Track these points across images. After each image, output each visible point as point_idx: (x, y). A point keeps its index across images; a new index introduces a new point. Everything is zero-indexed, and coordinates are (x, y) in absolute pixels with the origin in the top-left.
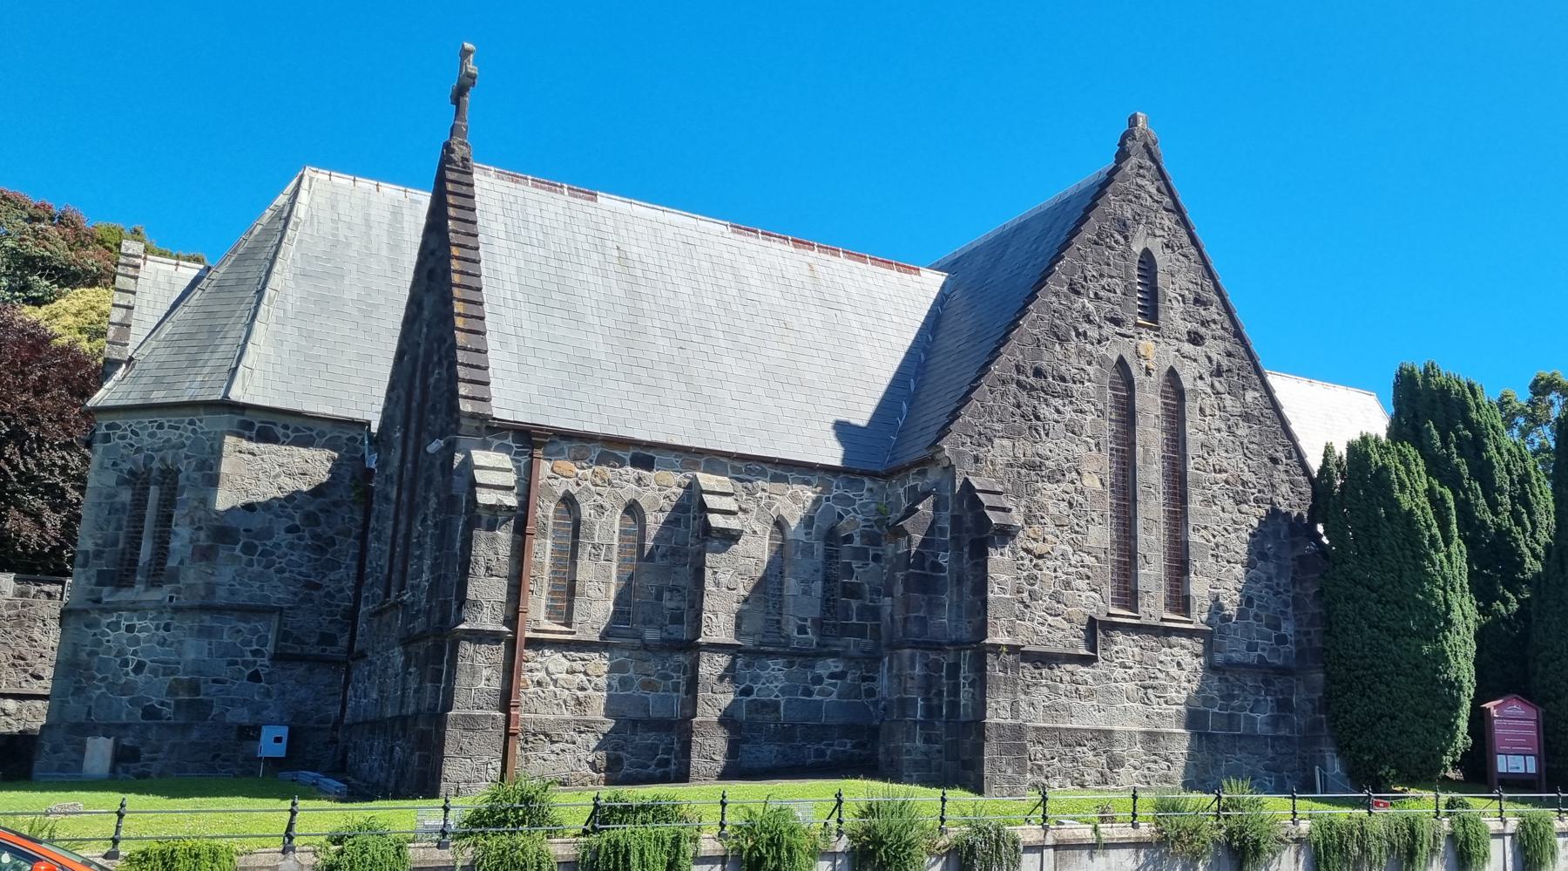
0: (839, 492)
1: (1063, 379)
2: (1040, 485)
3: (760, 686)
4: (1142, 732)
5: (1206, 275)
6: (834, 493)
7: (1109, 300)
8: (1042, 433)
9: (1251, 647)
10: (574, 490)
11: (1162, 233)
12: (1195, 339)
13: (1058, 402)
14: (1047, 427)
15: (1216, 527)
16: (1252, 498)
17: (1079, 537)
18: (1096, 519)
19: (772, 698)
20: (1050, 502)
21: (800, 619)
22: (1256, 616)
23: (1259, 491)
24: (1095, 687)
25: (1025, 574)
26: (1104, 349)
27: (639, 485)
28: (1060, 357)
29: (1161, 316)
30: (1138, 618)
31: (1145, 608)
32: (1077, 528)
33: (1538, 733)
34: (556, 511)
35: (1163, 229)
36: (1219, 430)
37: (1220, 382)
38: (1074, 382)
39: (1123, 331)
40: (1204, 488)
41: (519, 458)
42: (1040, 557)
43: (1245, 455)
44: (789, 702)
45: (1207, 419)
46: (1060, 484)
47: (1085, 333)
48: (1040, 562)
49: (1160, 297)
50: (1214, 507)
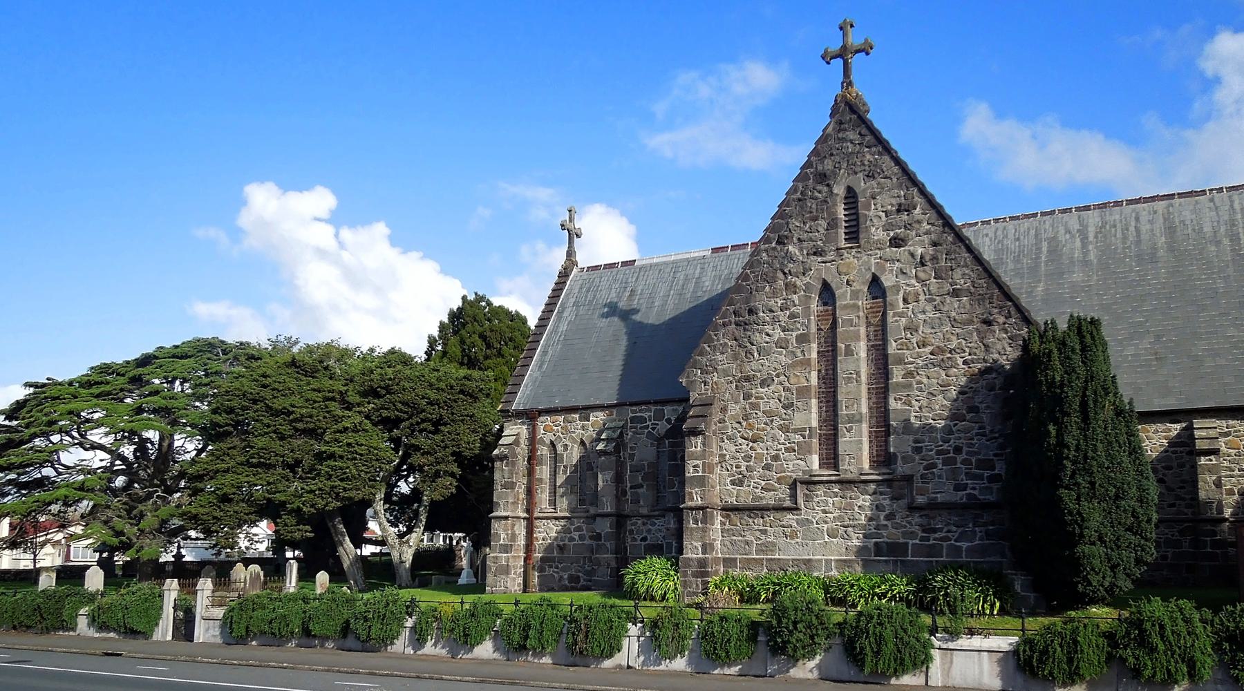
1: (772, 311)
2: (753, 392)
4: (837, 561)
5: (909, 184)
7: (811, 240)
9: (957, 488)
10: (553, 438)
11: (863, 168)
12: (897, 242)
15: (919, 393)
16: (960, 361)
18: (801, 407)
20: (761, 401)
23: (970, 354)
25: (743, 455)
26: (808, 279)
28: (770, 295)
29: (861, 236)
30: (839, 475)
31: (845, 467)
32: (784, 416)
35: (864, 164)
36: (924, 312)
37: (924, 271)
38: (781, 310)
40: (905, 364)
42: (754, 441)
45: (910, 306)
47: (790, 271)
48: (755, 445)
49: (862, 220)
50: (918, 377)
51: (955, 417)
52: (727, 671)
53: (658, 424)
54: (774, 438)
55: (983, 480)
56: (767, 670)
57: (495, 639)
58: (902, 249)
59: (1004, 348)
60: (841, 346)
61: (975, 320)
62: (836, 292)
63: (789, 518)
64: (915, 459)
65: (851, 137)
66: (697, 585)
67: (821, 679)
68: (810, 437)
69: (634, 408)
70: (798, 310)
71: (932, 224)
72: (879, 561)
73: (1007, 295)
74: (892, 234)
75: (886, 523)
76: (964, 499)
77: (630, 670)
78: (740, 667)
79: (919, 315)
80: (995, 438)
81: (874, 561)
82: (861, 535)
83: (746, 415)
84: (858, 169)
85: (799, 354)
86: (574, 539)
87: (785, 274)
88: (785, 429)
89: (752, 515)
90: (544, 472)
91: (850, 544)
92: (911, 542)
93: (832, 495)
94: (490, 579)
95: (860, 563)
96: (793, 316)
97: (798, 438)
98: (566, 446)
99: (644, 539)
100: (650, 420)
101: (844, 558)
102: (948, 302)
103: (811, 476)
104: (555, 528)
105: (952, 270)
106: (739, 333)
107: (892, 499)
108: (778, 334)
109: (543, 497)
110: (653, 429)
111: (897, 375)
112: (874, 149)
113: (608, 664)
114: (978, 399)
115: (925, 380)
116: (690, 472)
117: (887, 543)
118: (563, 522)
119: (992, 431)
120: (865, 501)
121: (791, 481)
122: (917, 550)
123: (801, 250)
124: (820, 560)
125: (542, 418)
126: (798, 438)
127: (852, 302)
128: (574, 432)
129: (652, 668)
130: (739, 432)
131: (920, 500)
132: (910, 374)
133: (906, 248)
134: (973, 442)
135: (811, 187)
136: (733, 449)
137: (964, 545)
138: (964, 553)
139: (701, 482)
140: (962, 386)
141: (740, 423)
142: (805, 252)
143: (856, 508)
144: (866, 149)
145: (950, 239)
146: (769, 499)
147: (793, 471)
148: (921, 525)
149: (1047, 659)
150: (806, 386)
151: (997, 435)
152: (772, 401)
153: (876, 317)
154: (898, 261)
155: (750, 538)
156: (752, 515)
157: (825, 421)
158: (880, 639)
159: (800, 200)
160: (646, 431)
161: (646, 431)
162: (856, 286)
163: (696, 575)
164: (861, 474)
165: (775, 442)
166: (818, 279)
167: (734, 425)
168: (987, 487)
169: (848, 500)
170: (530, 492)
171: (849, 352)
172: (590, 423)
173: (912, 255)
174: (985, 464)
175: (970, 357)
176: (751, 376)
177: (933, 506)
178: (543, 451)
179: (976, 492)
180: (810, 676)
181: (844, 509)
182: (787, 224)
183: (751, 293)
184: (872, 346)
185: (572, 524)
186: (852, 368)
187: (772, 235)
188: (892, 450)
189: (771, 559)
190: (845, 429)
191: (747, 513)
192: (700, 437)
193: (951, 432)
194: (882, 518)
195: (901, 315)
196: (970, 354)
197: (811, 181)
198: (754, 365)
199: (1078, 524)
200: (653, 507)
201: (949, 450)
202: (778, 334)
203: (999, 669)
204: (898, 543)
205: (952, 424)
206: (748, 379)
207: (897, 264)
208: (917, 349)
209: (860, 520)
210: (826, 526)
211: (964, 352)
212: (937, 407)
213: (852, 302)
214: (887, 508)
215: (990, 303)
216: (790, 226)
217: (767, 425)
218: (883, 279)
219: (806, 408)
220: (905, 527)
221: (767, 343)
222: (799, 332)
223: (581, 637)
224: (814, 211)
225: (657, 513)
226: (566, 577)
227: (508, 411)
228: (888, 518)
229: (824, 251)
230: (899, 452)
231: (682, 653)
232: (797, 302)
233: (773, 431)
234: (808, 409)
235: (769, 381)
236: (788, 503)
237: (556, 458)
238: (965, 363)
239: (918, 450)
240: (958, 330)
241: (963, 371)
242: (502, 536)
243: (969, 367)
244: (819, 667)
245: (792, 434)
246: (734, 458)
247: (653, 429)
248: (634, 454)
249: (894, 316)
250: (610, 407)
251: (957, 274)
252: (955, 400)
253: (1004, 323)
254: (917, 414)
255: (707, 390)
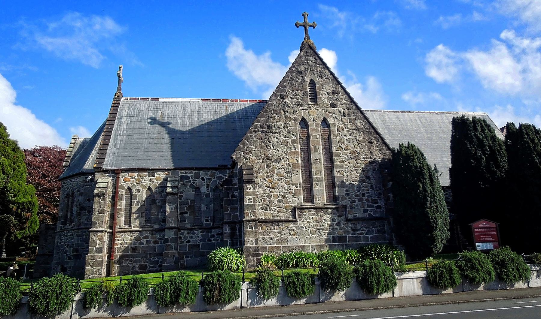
0: (218, 175)
3: (193, 240)
4: (317, 246)
5: (337, 83)
6: (216, 176)
7: (296, 98)
8: (272, 147)
9: (365, 211)
10: (130, 185)
12: (333, 105)
13: (277, 136)
14: (273, 145)
15: (346, 170)
16: (362, 157)
17: (288, 180)
18: (295, 173)
19: (197, 243)
20: (276, 169)
21: (206, 217)
22: (367, 200)
23: (365, 155)
24: (297, 231)
25: (267, 195)
26: (296, 115)
27: (151, 182)
28: (277, 120)
29: (318, 101)
30: (314, 205)
31: (317, 202)
33: (497, 233)
34: (126, 192)
36: (346, 136)
37: (345, 119)
38: (284, 128)
39: (303, 108)
40: (340, 157)
41: (113, 178)
43: (358, 143)
44: (203, 244)
46: (280, 163)
47: (287, 111)
48: (273, 190)
49: (318, 94)
50: (345, 163)
51: (361, 181)
52: (299, 302)
53: (196, 180)
54: (282, 187)
55: (374, 208)
56: (320, 299)
57: (148, 302)
58: (335, 109)
59: (378, 154)
60: (312, 147)
61: (366, 141)
62: (309, 123)
63: (292, 226)
64: (346, 199)
65: (311, 59)
66: (254, 261)
67: (347, 300)
68: (300, 187)
69: (183, 171)
70: (291, 129)
71: (347, 101)
72: (336, 245)
73: (378, 133)
74: (331, 102)
75: (337, 227)
76: (368, 216)
77: (243, 309)
78: (306, 299)
79: (344, 137)
80: (377, 190)
81: (334, 245)
82: (326, 233)
83: (268, 176)
84: (315, 73)
85: (293, 149)
86: (143, 244)
87: (284, 112)
88: (288, 183)
89: (273, 225)
90: (122, 205)
91: (321, 237)
92: (348, 235)
93: (312, 214)
94: (88, 269)
95: (328, 246)
96: (289, 131)
97: (294, 188)
98: (138, 190)
99: (189, 242)
100: (192, 178)
101: (319, 244)
102: (355, 133)
103: (301, 205)
104: (130, 237)
105: (356, 120)
106: (263, 136)
107: (338, 216)
108: (282, 139)
109: (121, 220)
110: (194, 183)
111: (337, 161)
112: (321, 66)
113: (228, 307)
114: (370, 174)
115: (348, 165)
116: (247, 202)
117: (338, 236)
118: (137, 234)
119: (376, 187)
120: (327, 217)
121: (292, 208)
122: (351, 239)
123: (292, 102)
124: (308, 246)
125: (123, 174)
126: (294, 188)
127: (316, 128)
128: (145, 183)
129: (256, 306)
130: (265, 183)
131: (350, 217)
132: (342, 161)
133: (337, 108)
134: (369, 191)
135: (295, 76)
136: (262, 192)
137: (370, 236)
138: (370, 240)
139: (253, 207)
140: (363, 168)
141: (265, 179)
142: (294, 104)
143: (323, 220)
144: (318, 66)
145: (354, 107)
146: (281, 216)
147: (292, 203)
148: (351, 228)
149: (442, 278)
150: (297, 164)
151: (377, 189)
152: (281, 170)
153: (326, 136)
154: (334, 113)
155: (272, 236)
156: (273, 225)
157: (305, 180)
158: (379, 277)
159: (290, 81)
160: (189, 184)
161: (189, 184)
162: (317, 121)
163: (253, 256)
164: (324, 205)
165: (282, 189)
166: (300, 116)
167: (262, 180)
168: (376, 211)
169: (320, 217)
170: (113, 216)
171: (316, 150)
172: (155, 178)
173: (340, 112)
174: (375, 201)
175: (365, 156)
176: (270, 157)
177: (356, 219)
178: (123, 193)
179: (372, 213)
180: (341, 299)
181: (318, 221)
182: (285, 90)
183: (268, 118)
184: (324, 148)
185: (141, 235)
186: (317, 157)
187: (277, 94)
188: (337, 194)
189: (285, 246)
190: (316, 184)
191: (270, 223)
192: (252, 184)
193: (360, 187)
194: (335, 225)
195: (337, 136)
196: (365, 155)
197: (295, 73)
198: (271, 152)
199: (435, 223)
200: (193, 224)
201: (360, 195)
202: (282, 139)
203: (421, 285)
204: (342, 236)
205: (360, 183)
206: (268, 158)
207: (334, 115)
208: (344, 151)
209: (325, 226)
210: (310, 229)
211: (363, 154)
212: (354, 176)
213: (316, 128)
214: (337, 220)
215: (371, 135)
216: (286, 91)
217: (279, 180)
218: (328, 120)
219: (297, 174)
220: (345, 229)
221: (277, 142)
222: (292, 139)
223: (216, 292)
224: (297, 86)
225: (196, 227)
226: (137, 266)
227: (101, 168)
228: (337, 225)
229: (303, 105)
230: (340, 195)
231: (274, 295)
232: (291, 125)
233: (282, 184)
234: (298, 174)
235: (279, 160)
236: (291, 218)
237: (131, 196)
238: (364, 158)
239: (348, 194)
240: (360, 145)
241: (363, 162)
242: (98, 243)
243: (365, 160)
244: (345, 294)
245: (291, 186)
246: (263, 196)
247: (194, 183)
248: (182, 196)
249: (334, 136)
250: (168, 170)
251: (358, 122)
252: (361, 174)
253: (377, 144)
254: (346, 179)
255: (247, 162)
